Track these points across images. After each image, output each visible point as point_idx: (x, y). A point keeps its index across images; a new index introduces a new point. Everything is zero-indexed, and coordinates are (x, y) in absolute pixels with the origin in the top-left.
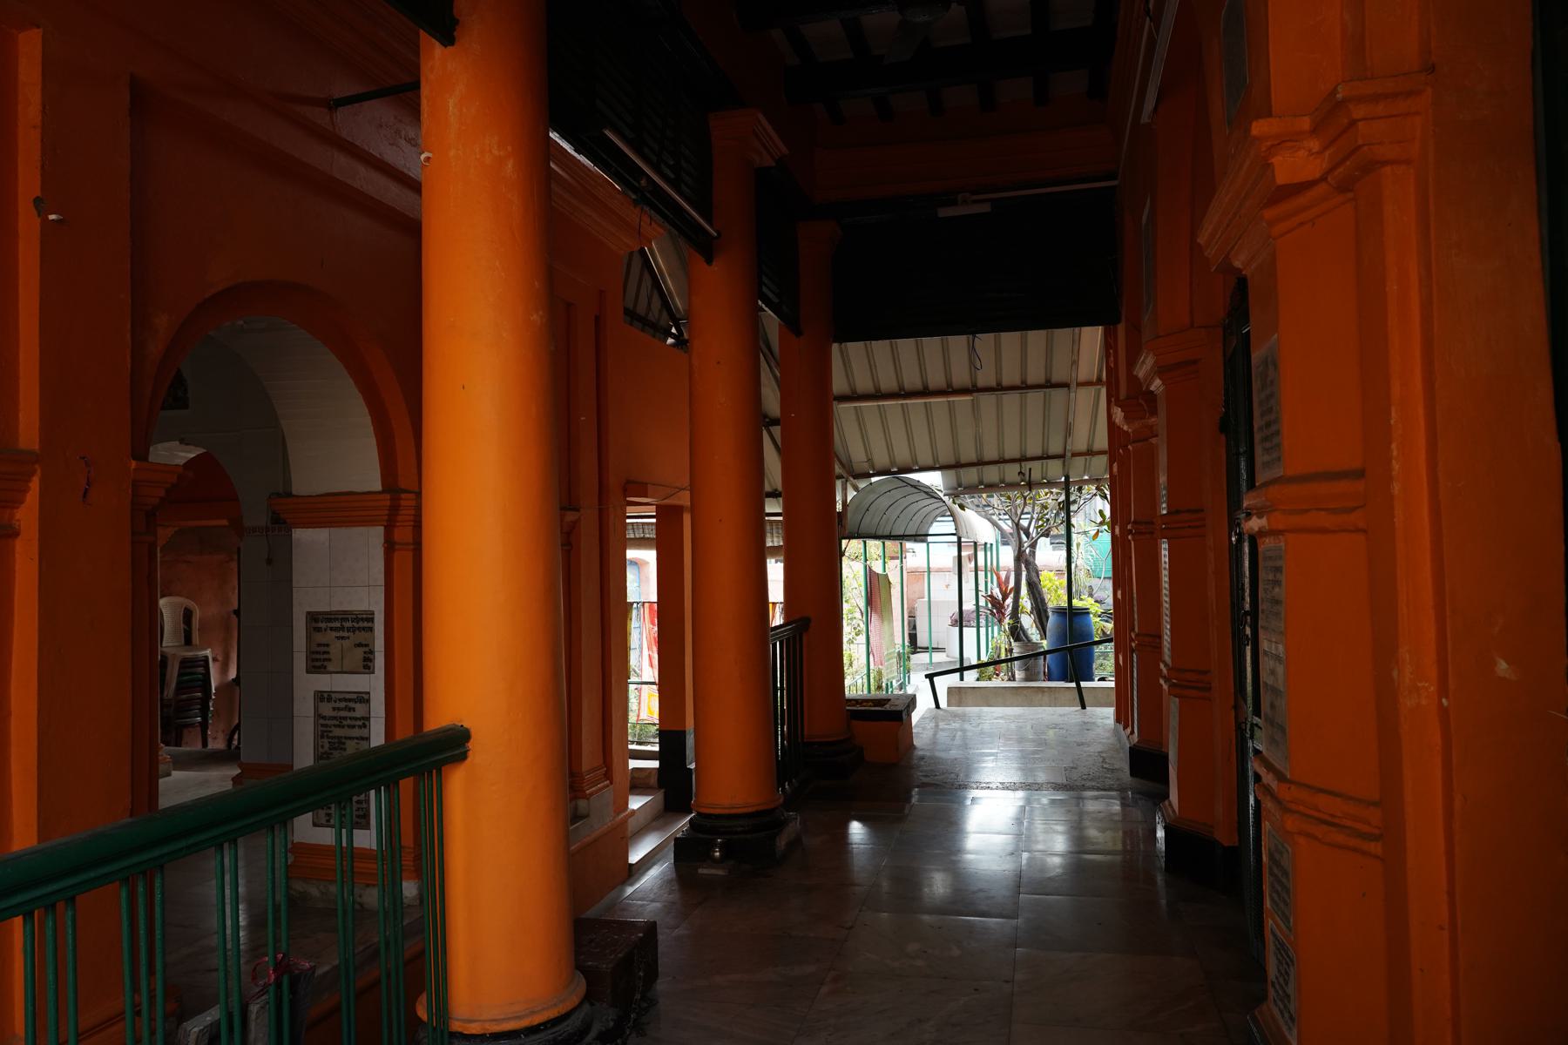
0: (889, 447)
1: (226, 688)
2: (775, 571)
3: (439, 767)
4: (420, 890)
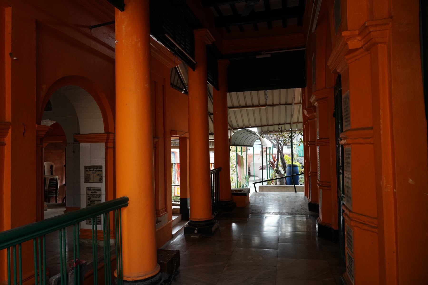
0: (243, 122)
1: (62, 187)
2: (212, 155)
3: (120, 208)
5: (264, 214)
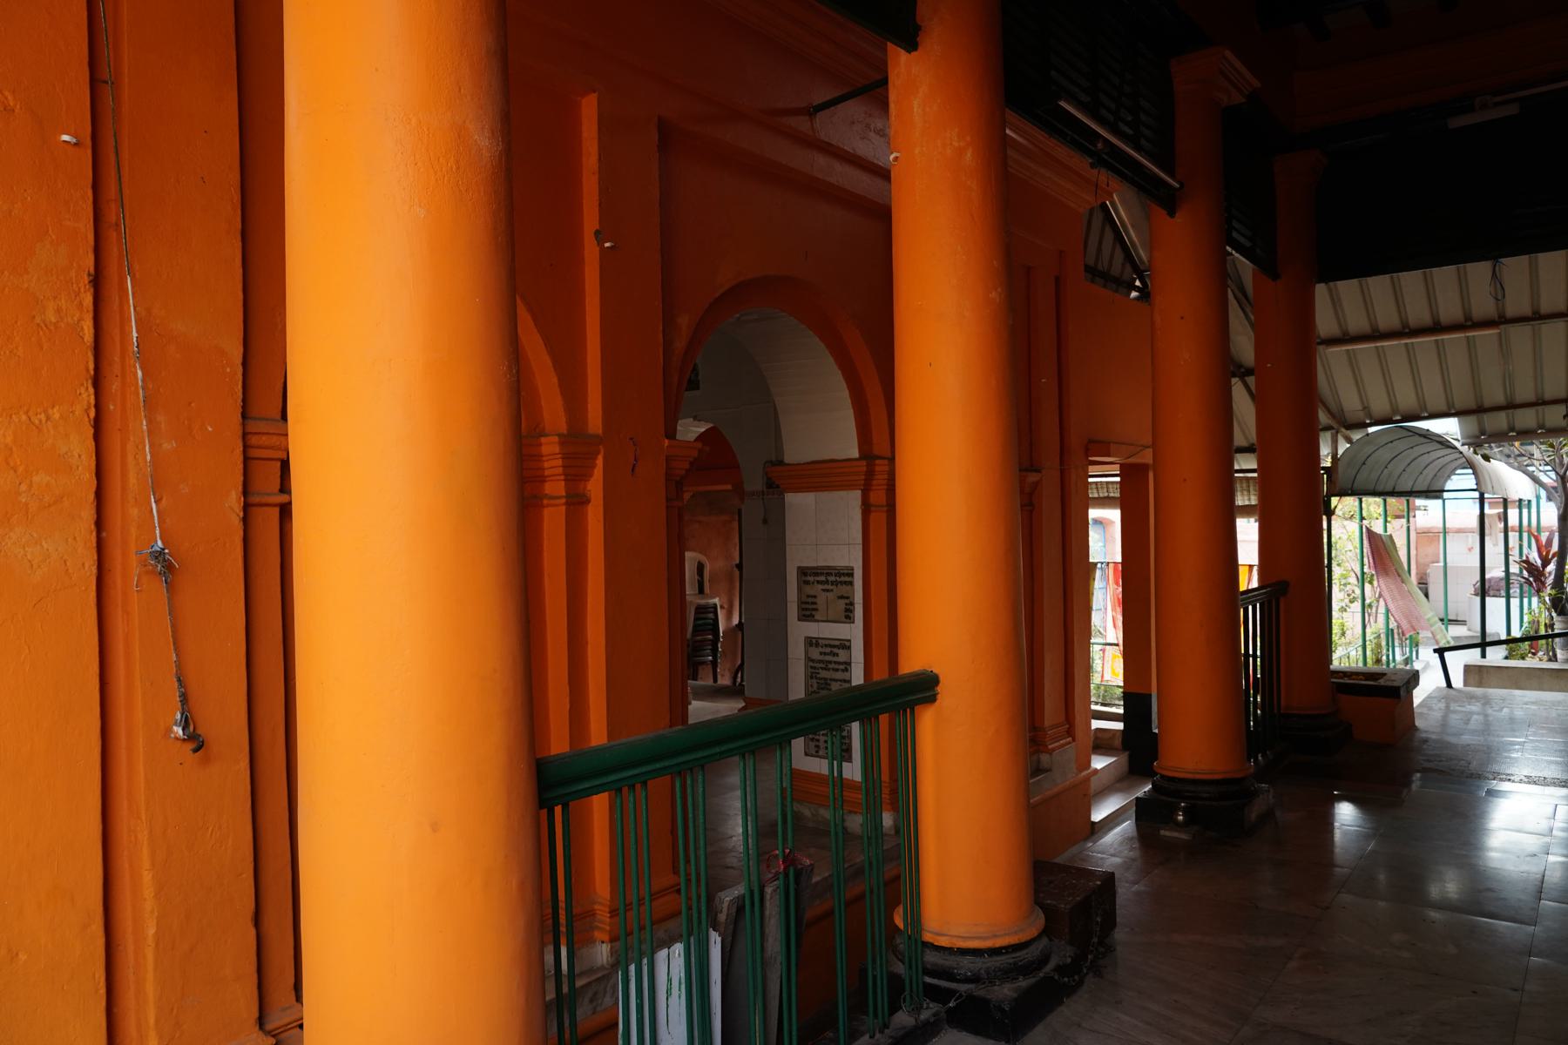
0: (1390, 392)
1: (731, 632)
2: (1248, 532)
3: (912, 706)
4: (895, 821)
5: (1497, 776)
